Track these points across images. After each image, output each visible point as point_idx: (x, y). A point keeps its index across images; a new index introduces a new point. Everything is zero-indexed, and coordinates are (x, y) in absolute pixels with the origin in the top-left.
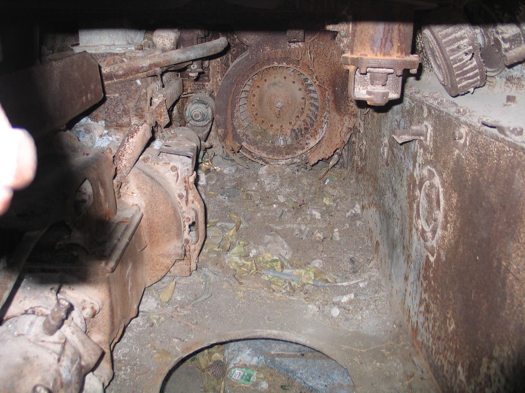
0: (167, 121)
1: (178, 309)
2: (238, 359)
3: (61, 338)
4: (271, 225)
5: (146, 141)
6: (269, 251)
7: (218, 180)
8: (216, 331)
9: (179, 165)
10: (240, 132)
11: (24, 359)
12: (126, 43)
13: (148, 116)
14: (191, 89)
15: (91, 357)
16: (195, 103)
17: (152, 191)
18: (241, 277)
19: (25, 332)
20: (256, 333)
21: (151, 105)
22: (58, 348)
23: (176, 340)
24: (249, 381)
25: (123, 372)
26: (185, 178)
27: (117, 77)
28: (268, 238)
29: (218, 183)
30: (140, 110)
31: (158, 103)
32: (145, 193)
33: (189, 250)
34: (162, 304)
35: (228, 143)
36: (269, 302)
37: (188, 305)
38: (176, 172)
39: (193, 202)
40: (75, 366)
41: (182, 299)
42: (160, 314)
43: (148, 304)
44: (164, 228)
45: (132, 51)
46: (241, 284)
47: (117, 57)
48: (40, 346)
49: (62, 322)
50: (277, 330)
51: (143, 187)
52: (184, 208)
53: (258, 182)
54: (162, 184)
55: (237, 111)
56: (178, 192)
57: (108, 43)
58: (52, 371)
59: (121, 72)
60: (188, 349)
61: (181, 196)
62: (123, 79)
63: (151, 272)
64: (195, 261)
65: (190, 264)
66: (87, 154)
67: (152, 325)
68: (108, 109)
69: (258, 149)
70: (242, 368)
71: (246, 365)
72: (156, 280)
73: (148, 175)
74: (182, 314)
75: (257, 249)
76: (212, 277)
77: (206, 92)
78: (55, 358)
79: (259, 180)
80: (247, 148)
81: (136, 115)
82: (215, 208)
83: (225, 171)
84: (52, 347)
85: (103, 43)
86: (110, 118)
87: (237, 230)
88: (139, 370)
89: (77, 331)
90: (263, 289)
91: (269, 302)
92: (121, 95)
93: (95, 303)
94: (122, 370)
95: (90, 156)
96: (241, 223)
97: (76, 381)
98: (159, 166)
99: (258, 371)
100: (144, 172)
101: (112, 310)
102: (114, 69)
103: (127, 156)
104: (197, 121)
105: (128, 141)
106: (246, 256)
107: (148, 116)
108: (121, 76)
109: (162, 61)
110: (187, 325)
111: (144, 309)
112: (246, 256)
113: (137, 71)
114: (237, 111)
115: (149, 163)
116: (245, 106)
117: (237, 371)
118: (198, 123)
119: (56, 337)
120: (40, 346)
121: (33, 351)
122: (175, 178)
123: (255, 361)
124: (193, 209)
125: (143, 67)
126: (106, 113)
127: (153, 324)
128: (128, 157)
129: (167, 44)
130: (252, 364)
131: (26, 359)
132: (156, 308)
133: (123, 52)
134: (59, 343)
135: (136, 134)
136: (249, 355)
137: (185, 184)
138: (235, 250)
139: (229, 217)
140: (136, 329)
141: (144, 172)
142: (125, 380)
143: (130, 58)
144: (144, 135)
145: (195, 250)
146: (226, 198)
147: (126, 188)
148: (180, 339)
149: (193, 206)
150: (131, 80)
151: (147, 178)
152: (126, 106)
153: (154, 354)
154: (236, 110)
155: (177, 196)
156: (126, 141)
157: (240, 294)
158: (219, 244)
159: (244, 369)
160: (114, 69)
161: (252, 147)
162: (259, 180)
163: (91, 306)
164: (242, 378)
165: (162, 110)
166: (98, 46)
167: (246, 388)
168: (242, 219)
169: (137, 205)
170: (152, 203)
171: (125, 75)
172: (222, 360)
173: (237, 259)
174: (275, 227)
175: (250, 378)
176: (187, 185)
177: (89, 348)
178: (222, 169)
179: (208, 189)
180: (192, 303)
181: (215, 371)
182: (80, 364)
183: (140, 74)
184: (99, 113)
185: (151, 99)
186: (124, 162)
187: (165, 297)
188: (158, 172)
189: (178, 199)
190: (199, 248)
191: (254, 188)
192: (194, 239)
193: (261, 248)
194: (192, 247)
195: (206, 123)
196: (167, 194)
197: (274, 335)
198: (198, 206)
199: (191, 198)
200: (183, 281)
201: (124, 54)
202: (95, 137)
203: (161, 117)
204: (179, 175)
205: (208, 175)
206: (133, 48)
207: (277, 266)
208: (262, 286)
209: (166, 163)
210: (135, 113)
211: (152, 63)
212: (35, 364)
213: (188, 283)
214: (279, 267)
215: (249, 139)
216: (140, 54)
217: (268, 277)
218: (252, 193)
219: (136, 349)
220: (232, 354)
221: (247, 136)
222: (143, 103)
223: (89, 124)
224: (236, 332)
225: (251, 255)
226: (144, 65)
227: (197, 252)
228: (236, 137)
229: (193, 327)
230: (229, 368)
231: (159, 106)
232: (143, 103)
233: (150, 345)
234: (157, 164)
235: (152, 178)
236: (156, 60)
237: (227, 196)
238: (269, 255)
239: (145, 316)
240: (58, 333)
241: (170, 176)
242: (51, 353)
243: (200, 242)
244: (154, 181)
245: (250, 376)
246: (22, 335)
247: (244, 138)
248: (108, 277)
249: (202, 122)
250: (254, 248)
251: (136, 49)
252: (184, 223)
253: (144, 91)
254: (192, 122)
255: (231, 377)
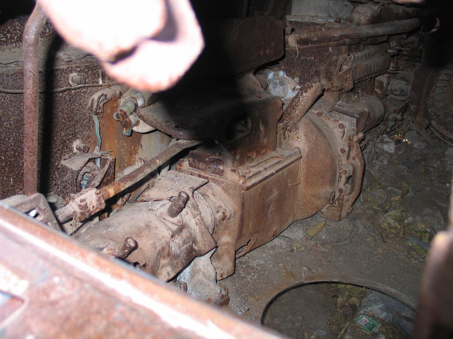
0: (351, 86)
1: (318, 245)
2: (370, 308)
3: (178, 222)
4: (437, 201)
5: (316, 97)
6: (424, 222)
7: (405, 152)
8: (343, 273)
9: (347, 124)
10: (432, 111)
11: (146, 226)
12: (326, 15)
13: (335, 80)
14: (403, 68)
15: (205, 247)
16: (398, 79)
17: (317, 140)
18: (387, 237)
19: (155, 209)
20: (376, 285)
21: (340, 70)
22: (175, 228)
23: (305, 268)
24: (371, 329)
25: (250, 276)
26: (350, 136)
27: (313, 42)
28: (428, 210)
29: (406, 154)
30: (329, 74)
31: (345, 70)
32: (310, 141)
33: (343, 199)
34: (308, 238)
35: (418, 119)
36: (402, 264)
37: (328, 244)
38: (343, 130)
39: (354, 159)
40: (185, 246)
41: (326, 238)
42: (302, 245)
43: (296, 234)
44: (320, 173)
45: (331, 23)
46: (385, 242)
47: (317, 26)
48: (162, 222)
49: (181, 209)
50: (396, 289)
51: (309, 136)
52: (344, 161)
53: (441, 161)
54: (327, 136)
55: (433, 91)
56: (342, 147)
57: (313, 14)
58: (163, 241)
59: (315, 39)
60: (311, 278)
61: (343, 151)
62: (317, 45)
63: (303, 207)
64: (347, 210)
65: (341, 212)
66: (260, 97)
67: (292, 250)
68: (304, 69)
69: (446, 130)
70: (370, 317)
71: (374, 316)
72: (307, 216)
73: (317, 127)
74: (320, 250)
75: (413, 217)
76: (361, 229)
77: (411, 71)
78: (170, 234)
79: (442, 159)
80: (436, 127)
81: (326, 77)
82: (391, 174)
83: (415, 145)
84: (170, 225)
85: (309, 14)
86: (304, 76)
87: (402, 197)
88: (263, 280)
89: (201, 224)
90: (403, 252)
91: (402, 264)
92: (315, 58)
93: (228, 210)
94: (251, 275)
95: (260, 99)
96: (408, 192)
97: (184, 257)
98: (329, 122)
99: (383, 325)
100: (313, 123)
101: (242, 220)
102: (310, 35)
103: (300, 107)
104: (396, 95)
105: (302, 95)
106: (400, 221)
107: (335, 80)
108: (315, 42)
109: (352, 33)
110: (321, 260)
111: (291, 237)
112: (401, 221)
113: (329, 39)
114: (433, 91)
115: (322, 118)
116: (445, 88)
117: (364, 318)
118: (397, 97)
119: (175, 220)
120: (162, 222)
121: (155, 222)
122: (341, 135)
123: (383, 315)
124: (352, 165)
125: (334, 37)
126: (302, 72)
127: (293, 250)
128: (300, 108)
129: (362, 20)
130: (380, 317)
131: (148, 226)
132: (301, 239)
133: (323, 22)
134: (176, 225)
135: (309, 90)
136: (381, 308)
137: (349, 141)
138: (392, 213)
139: (401, 185)
140: (278, 250)
141: (313, 123)
142: (249, 283)
143: (328, 29)
144: (316, 92)
145: (348, 200)
146: (406, 168)
147: (295, 133)
148: (309, 268)
149: (353, 162)
150: (324, 47)
151: (315, 129)
152: (317, 68)
153: (282, 272)
154: (432, 90)
155: (339, 150)
156: (300, 94)
157: (380, 250)
158: (382, 204)
159: (371, 319)
160: (310, 35)
161: (440, 127)
162: (442, 159)
163: (223, 211)
164: (366, 325)
165: (348, 76)
166: (304, 16)
167: (365, 334)
168: (410, 189)
169: (298, 148)
170: (314, 150)
171: (319, 41)
172: (358, 305)
173: (391, 221)
174: (440, 204)
175: (373, 328)
176: (351, 142)
177: (206, 239)
178: (413, 142)
179: (394, 157)
180: (333, 244)
181: (346, 312)
182: (191, 247)
183: (332, 43)
184: (296, 71)
185: (341, 66)
186: (297, 112)
187: (312, 232)
188: (328, 127)
189: (340, 153)
190: (353, 200)
191: (435, 166)
192: (348, 191)
193: (418, 218)
194: (346, 197)
195: (405, 98)
196: (329, 146)
197: (391, 293)
198: (358, 163)
199: (352, 154)
200: (333, 224)
201: (324, 24)
202: (287, 90)
203: (346, 82)
204: (346, 132)
205: (398, 145)
206: (332, 21)
207: (425, 236)
208: (403, 249)
209: (336, 120)
210: (325, 75)
211: (343, 34)
212: (153, 232)
213: (337, 227)
214: (427, 238)
215: (439, 119)
216: (337, 26)
217: (412, 243)
218: (431, 169)
219: (270, 264)
220: (367, 303)
221: (438, 116)
222: (332, 69)
223: (284, 78)
224: (360, 279)
225: (406, 221)
226: (335, 35)
227: (350, 203)
228: (427, 115)
229: (325, 263)
230: (359, 313)
231: (345, 73)
232: (332, 69)
233: (282, 265)
234: (329, 119)
235: (319, 130)
236: (346, 32)
237: (407, 166)
238: (424, 226)
239: (289, 242)
240: (178, 217)
241: (337, 132)
242: (168, 230)
243: (354, 195)
244: (319, 131)
245: (374, 326)
246: (152, 210)
247: (435, 117)
248: (243, 194)
249: (401, 97)
250: (412, 216)
251: (335, 22)
252: (340, 173)
253: (335, 58)
254: (392, 96)
255: (357, 321)
